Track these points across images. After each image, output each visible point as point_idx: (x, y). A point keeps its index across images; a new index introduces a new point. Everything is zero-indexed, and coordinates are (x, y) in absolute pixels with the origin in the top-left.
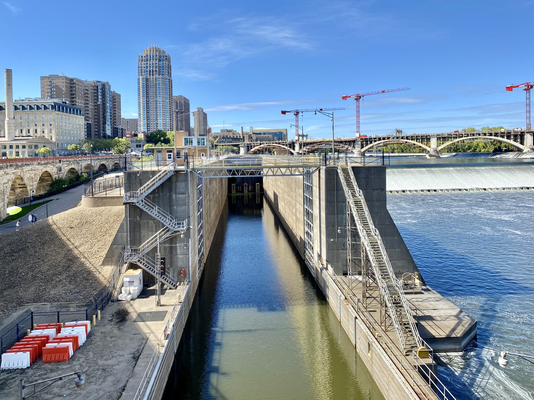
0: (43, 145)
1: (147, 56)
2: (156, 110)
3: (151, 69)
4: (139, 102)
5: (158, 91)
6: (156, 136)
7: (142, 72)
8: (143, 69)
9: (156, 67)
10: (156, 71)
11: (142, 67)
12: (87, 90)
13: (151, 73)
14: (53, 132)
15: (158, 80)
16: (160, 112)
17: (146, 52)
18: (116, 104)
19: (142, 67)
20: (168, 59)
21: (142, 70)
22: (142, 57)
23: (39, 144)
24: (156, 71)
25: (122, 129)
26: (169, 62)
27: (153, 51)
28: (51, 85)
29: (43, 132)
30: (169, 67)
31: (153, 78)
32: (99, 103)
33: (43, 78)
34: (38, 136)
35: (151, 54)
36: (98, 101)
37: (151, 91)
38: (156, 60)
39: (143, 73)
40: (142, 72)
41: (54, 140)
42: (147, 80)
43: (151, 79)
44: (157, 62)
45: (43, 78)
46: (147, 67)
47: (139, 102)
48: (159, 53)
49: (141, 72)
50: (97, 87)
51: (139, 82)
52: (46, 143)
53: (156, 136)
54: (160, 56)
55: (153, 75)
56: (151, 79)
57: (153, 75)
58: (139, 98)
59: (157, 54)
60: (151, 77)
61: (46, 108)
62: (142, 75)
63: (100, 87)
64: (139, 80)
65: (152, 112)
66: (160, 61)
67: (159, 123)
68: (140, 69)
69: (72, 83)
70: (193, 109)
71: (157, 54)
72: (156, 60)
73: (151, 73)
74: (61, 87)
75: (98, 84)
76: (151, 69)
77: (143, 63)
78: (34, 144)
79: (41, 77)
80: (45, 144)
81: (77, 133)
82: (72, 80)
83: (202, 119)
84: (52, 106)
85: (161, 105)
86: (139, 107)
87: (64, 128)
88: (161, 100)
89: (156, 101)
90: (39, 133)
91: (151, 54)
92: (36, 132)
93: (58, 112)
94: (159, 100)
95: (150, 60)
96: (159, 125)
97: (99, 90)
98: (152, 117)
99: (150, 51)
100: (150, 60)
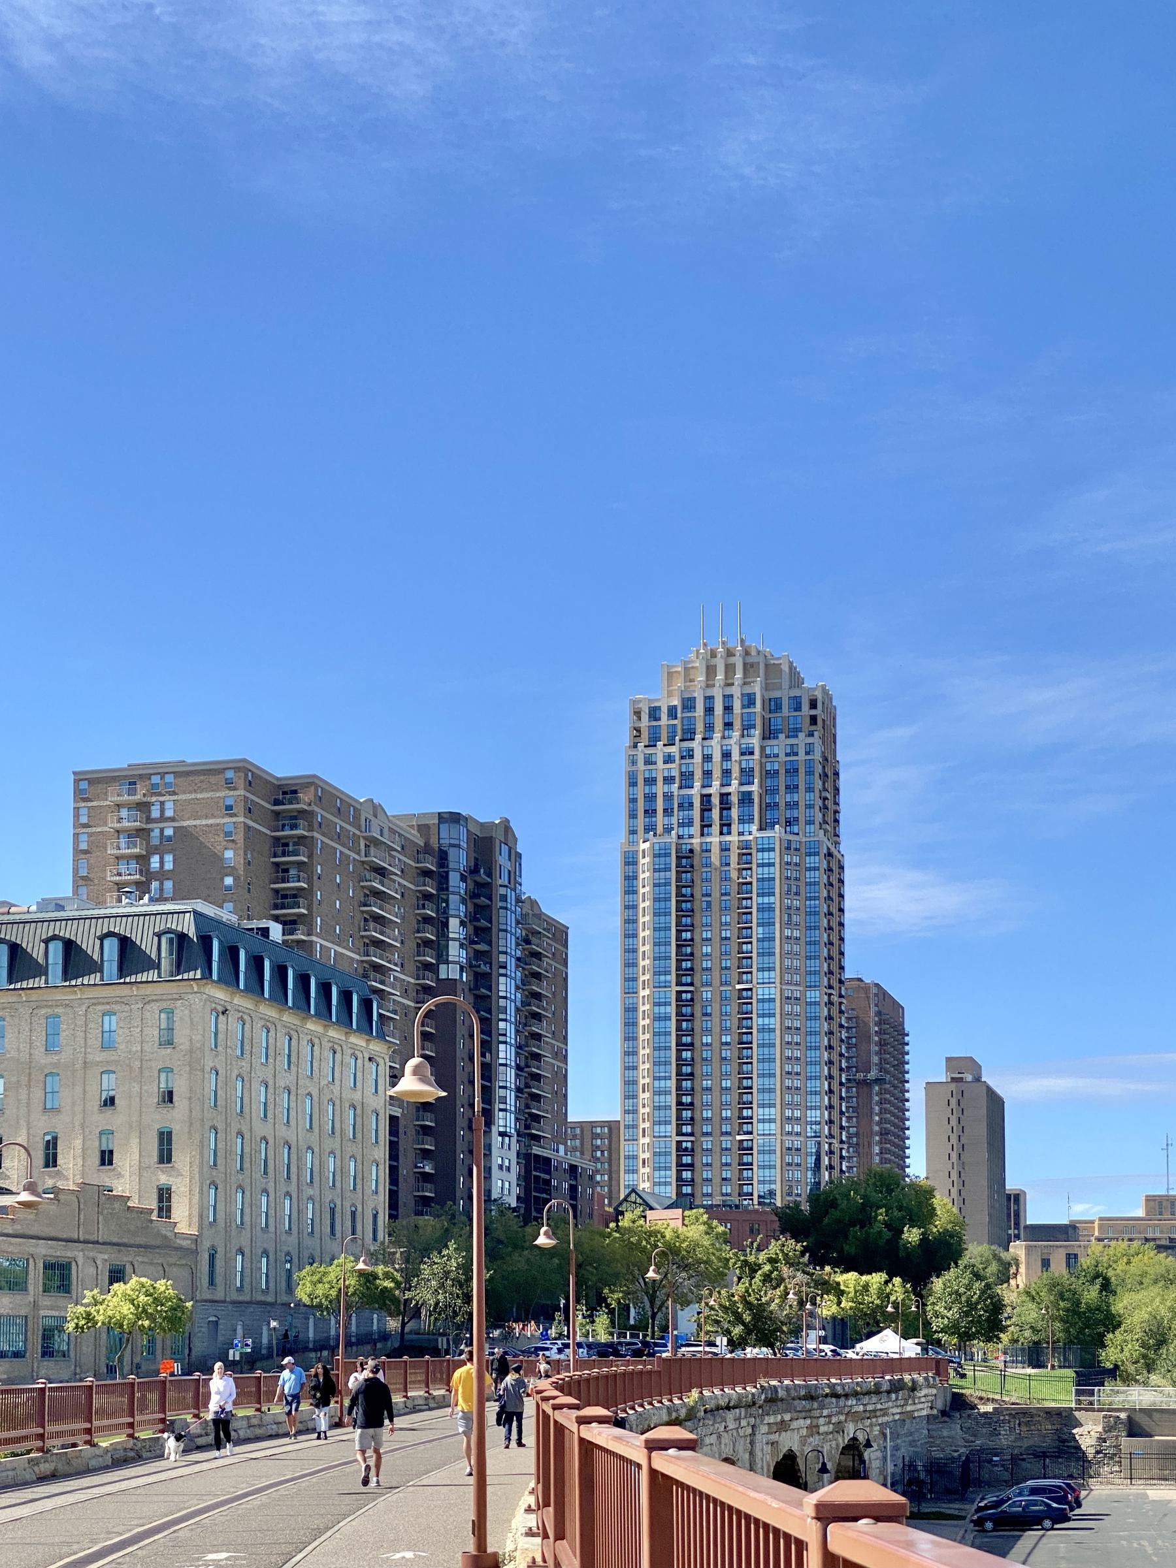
0: (104, 1258)
1: (689, 704)
2: (744, 1061)
3: (734, 787)
4: (630, 1011)
5: (757, 932)
6: (863, 1216)
7: (650, 812)
8: (660, 789)
9: (747, 775)
10: (746, 799)
11: (650, 781)
12: (381, 872)
13: (717, 811)
14: (183, 1157)
15: (757, 857)
16: (769, 1076)
17: (679, 683)
18: (543, 989)
19: (650, 781)
20: (818, 716)
21: (650, 798)
22: (654, 713)
23: (78, 1254)
24: (746, 799)
25: (573, 1168)
26: (830, 740)
27: (730, 669)
28: (141, 833)
29: (106, 1158)
30: (830, 775)
31: (725, 849)
32: (449, 972)
33: (89, 785)
34: (69, 1184)
35: (718, 694)
36: (442, 956)
37: (714, 931)
38: (747, 727)
39: (660, 820)
40: (650, 812)
41: (184, 1218)
42: (686, 859)
43: (715, 858)
44: (755, 741)
45: (89, 785)
46: (687, 779)
47: (630, 1011)
48: (767, 687)
49: (644, 811)
50: (443, 858)
51: (630, 879)
52: (136, 1239)
53: (863, 1216)
54: (773, 705)
55: (726, 827)
56: (715, 858)
57: (726, 827)
58: (630, 982)
59: (757, 689)
60: (715, 839)
61: (130, 957)
62: (650, 828)
63: (460, 860)
64: (630, 861)
65: (715, 1080)
66: (769, 734)
67: (758, 1142)
68: (641, 791)
69: (286, 815)
70: (924, 1070)
71: (757, 689)
72: (747, 727)
73: (717, 811)
74: (215, 842)
75: (448, 835)
76: (715, 789)
77: (660, 750)
78: (43, 1250)
79: (79, 777)
80: (123, 1258)
81: (343, 1171)
82: (286, 792)
83: (980, 1130)
84: (182, 937)
85: (775, 1023)
86: (630, 1037)
87: (261, 1129)
88: (774, 992)
89: (744, 997)
90: (74, 1167)
91: (718, 694)
92: (51, 1160)
93: (220, 994)
94: (760, 992)
95: (709, 728)
96: (756, 1158)
97: (454, 879)
98: (714, 1107)
99: (711, 671)
100: (709, 728)
